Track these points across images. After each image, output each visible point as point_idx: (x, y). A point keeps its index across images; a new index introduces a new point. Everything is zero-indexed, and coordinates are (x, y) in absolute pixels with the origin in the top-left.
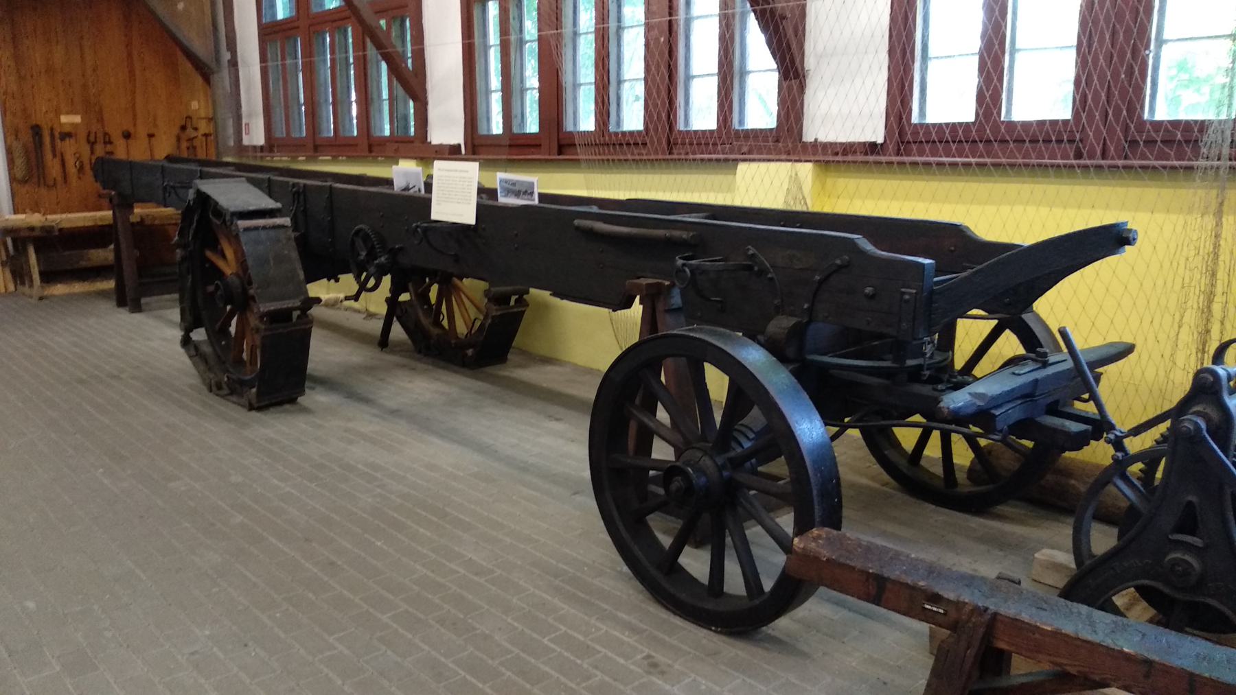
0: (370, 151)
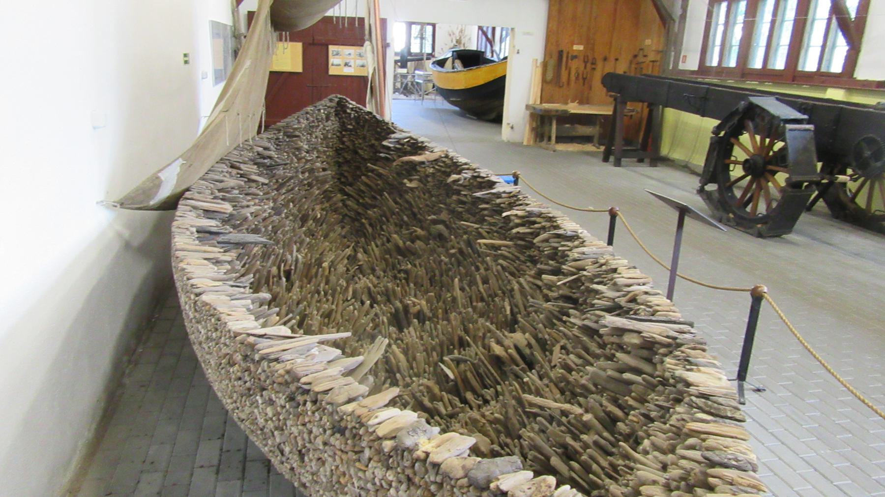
0: (793, 81)
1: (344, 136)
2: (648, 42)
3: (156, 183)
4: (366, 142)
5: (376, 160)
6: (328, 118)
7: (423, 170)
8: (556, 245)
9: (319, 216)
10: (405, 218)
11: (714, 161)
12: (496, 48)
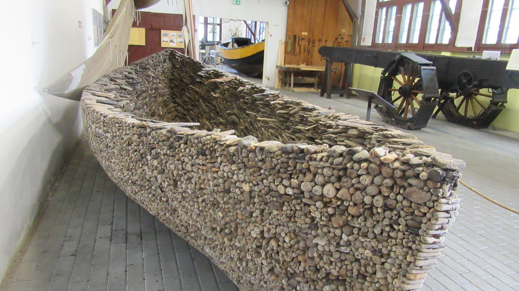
0: (423, 48)
1: (174, 72)
2: (343, 31)
3: (69, 79)
4: (187, 74)
5: (194, 83)
6: (165, 61)
7: (222, 87)
8: (302, 114)
9: (161, 113)
10: (212, 115)
11: (383, 90)
12: (257, 37)
